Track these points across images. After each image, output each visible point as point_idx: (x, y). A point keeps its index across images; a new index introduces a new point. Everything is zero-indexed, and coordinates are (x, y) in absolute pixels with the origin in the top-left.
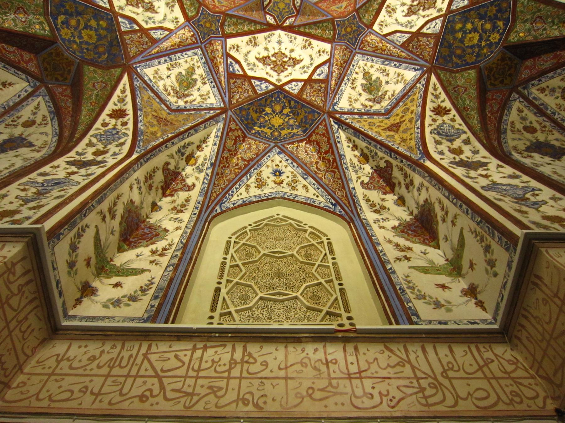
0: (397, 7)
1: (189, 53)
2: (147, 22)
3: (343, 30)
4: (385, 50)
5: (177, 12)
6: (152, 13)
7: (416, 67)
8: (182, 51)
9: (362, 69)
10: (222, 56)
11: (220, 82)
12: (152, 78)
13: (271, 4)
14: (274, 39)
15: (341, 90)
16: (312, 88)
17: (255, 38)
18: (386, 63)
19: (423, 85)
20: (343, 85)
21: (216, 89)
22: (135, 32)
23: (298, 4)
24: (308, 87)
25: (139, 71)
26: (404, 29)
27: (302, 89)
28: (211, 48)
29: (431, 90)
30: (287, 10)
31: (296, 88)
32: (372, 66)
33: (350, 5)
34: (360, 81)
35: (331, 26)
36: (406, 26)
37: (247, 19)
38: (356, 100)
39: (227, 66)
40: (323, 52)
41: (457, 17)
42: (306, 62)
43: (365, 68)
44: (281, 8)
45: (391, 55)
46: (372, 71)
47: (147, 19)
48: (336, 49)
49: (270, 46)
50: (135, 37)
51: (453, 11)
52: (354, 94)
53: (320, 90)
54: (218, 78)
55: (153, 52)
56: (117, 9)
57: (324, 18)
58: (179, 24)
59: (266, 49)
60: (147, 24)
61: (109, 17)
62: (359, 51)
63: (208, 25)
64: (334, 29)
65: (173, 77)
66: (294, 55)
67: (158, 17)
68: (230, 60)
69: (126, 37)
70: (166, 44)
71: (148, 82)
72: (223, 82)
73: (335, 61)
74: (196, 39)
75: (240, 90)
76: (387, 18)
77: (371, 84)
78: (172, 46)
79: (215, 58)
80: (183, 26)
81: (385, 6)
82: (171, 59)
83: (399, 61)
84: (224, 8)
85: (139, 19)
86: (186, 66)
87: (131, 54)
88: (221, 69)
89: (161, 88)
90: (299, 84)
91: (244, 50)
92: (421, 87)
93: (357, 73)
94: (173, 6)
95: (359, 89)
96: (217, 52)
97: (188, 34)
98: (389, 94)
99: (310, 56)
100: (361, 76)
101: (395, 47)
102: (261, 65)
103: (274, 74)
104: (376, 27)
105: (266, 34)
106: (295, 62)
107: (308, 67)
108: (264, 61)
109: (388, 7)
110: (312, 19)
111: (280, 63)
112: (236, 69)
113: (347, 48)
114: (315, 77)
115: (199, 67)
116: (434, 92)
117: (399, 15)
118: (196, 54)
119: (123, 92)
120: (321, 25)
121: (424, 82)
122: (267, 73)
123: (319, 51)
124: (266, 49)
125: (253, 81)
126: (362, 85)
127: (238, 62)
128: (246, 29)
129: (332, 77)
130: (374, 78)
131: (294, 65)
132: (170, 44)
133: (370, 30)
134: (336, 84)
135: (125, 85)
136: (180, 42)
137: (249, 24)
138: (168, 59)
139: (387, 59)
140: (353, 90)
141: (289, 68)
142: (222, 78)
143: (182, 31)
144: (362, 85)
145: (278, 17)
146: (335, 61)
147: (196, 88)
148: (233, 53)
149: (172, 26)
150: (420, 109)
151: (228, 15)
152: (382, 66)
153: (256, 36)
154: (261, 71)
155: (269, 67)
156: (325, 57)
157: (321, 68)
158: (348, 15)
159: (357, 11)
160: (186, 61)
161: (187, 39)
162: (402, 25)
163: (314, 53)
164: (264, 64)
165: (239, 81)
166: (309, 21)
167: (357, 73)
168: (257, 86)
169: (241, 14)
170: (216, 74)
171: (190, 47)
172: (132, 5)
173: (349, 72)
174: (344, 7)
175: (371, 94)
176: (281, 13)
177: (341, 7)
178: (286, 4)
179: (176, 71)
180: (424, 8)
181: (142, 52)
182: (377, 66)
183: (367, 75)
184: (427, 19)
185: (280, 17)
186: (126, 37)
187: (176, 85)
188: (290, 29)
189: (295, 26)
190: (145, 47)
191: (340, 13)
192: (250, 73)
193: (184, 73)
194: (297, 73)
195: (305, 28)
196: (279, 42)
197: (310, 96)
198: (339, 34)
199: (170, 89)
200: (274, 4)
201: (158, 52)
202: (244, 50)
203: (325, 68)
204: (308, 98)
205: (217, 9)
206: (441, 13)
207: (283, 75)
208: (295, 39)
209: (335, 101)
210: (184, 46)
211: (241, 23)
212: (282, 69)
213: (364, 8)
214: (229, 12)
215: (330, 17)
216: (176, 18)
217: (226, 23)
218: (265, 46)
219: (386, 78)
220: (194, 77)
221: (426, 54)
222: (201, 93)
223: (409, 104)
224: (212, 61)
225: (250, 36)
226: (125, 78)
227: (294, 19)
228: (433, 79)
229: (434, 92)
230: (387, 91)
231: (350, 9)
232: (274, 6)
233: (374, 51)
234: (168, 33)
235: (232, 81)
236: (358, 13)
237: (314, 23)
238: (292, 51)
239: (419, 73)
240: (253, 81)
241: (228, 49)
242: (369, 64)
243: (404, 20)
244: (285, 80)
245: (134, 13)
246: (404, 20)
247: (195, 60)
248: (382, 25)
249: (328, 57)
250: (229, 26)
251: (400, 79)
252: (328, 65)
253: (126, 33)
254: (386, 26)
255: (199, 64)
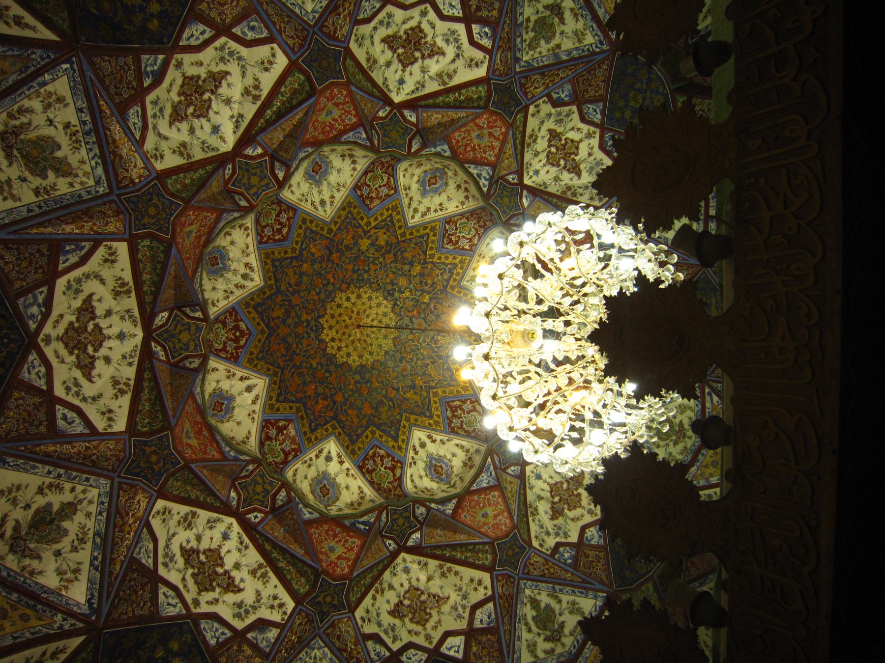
0: (194, 530)
1: (100, 171)
2: (155, 103)
3: (153, 448)
4: (121, 531)
5: (171, 161)
6: (171, 116)
7: (95, 601)
8: (102, 156)
9: (81, 496)
10: (96, 233)
11: (41, 224)
12: (49, 88)
13: (186, 320)
14: (127, 327)
15: (35, 467)
16: (37, 407)
17: (128, 292)
18: (98, 540)
19: (61, 627)
20: (47, 468)
21: (25, 213)
22: (141, 81)
23: (188, 365)
24: (37, 400)
25: (65, 66)
26: (161, 552)
27: (31, 389)
28: (110, 212)
29: (52, 647)
30: (178, 347)
31: (33, 376)
32: (88, 515)
33: (194, 453)
34: (56, 500)
35: (157, 426)
36: (166, 555)
37: (162, 278)
38: (14, 502)
39: (76, 241)
40: (110, 419)
41: (189, 636)
42: (89, 389)
43: (85, 502)
44: (181, 337)
45: (114, 545)
46: (79, 517)
47: (160, 104)
48: (299, 614)
49: (115, 319)
50: (131, 76)
51: (197, 625)
52: (25, 496)
53: (31, 424)
54: (49, 221)
55: (102, 103)
56: (179, 56)
57: (171, 413)
58: (152, 160)
59: (109, 313)
60: (152, 103)
61: (165, 40)
62: (116, 485)
63: (152, 211)
64: (152, 433)
65: (50, 131)
66: (100, 365)
67: (163, 126)
68: (87, 245)
69: (130, 59)
70: (116, 131)
71: (40, 79)
72: (42, 229)
73: (95, 443)
74: (127, 186)
75: (24, 264)
76: (176, 518)
77: (52, 521)
78: (114, 141)
79: (92, 217)
80: (149, 166)
81: (194, 509)
82: (87, 133)
83: (103, 565)
84: (181, 241)
85: (159, 92)
86: (73, 160)
87: (98, 60)
88: (68, 229)
89: (26, 103)
90: (43, 381)
91: (107, 273)
92: (56, 626)
93: (73, 490)
94: (181, 154)
95: (41, 501)
96: (102, 222)
97: (135, 174)
98: (35, 564)
99: (100, 396)
100: (68, 497)
101: (128, 548)
102: (77, 303)
103: (61, 330)
104: (160, 504)
105: (136, 313)
106: (87, 368)
107: (77, 394)
108: (87, 310)
109: (194, 514)
110: (166, 390)
111: (84, 339)
112: (70, 256)
113: (121, 461)
114: (60, 410)
115: (71, 185)
116: (48, 655)
117: (184, 537)
118: (98, 183)
119: (18, 21)
120: (158, 408)
121: (67, 627)
122: (61, 316)
123: (110, 411)
124: (109, 313)
125: (45, 289)
126: (50, 505)
127: (83, 261)
128: (146, 277)
129: (62, 444)
130: (66, 524)
131: (79, 366)
132: (117, 138)
133: (155, 494)
134: (48, 455)
135: (34, 29)
136: (121, 157)
137: (154, 282)
138: (87, 128)
139: (105, 540)
140: (35, 490)
141: (73, 358)
142: (49, 230)
143: (140, 163)
144: (50, 505)
145: (166, 331)
146: (95, 443)
147: (27, 174)
148: (101, 252)
149: (149, 145)
150: (9, 641)
151: (170, 247)
152: (91, 534)
153: (133, 294)
154: (65, 305)
155: (73, 318)
156: (100, 424)
157: (78, 421)
158: (179, 453)
159: (187, 467)
160: (83, 162)
161: (127, 171)
162: (167, 546)
163: (107, 401)
164: (80, 310)
165: (43, 261)
166: (162, 385)
167: (73, 490)
168: (35, 297)
169: (172, 270)
170: (58, 218)
171: (111, 173)
172: (182, 86)
173: (75, 474)
174: (190, 442)
175: (30, 527)
176: (173, 336)
177: (189, 438)
178: (187, 344)
179: (63, 140)
180: (197, 575)
181: (102, 82)
182: (90, 524)
183: (69, 509)
184: (181, 587)
185: (166, 336)
186: (130, 59)
187: (32, 135)
188: (146, 353)
189: (152, 363)
190: (112, 90)
191: (181, 438)
192: (61, 283)
193: (59, 154)
194: (64, 372)
195: (150, 380)
196: (121, 336)
197: (17, 407)
198: (145, 443)
199: (24, 120)
200: (188, 324)
201: (101, 111)
202: (107, 273)
203: (79, 428)
204: (12, 403)
205: (178, 229)
206: (192, 606)
207: (61, 347)
208: (130, 364)
209: (10, 460)
210: (113, 162)
211: (154, 269)
212: (71, 345)
213: (191, 476)
214: (174, 250)
215: (173, 422)
216: (162, 157)
217: (155, 244)
218: (115, 310)
219: (69, 548)
220: (51, 174)
221: (122, 608)
222: (16, 184)
223: (15, 616)
224: (86, 212)
225: (131, 284)
226: (46, 34)
227: (164, 358)
228: (75, 642)
229: (48, 655)
230: (39, 558)
231: (188, 453)
232: (183, 325)
233: (118, 511)
234: (138, 136)
235: (44, 248)
236: (181, 469)
237: (159, 397)
238: (107, 360)
239: (85, 609)
240: (45, 289)
241: (109, 243)
242: (93, 508)
243: (175, 548)
244: (49, 352)
245: (171, 85)
246: (175, 548)
247: (85, 179)
248: (164, 513)
249: (101, 430)
250: (151, 248)
251: (69, 575)
252: (86, 431)
253: (138, 62)
254: (164, 521)
255: (78, 187)
